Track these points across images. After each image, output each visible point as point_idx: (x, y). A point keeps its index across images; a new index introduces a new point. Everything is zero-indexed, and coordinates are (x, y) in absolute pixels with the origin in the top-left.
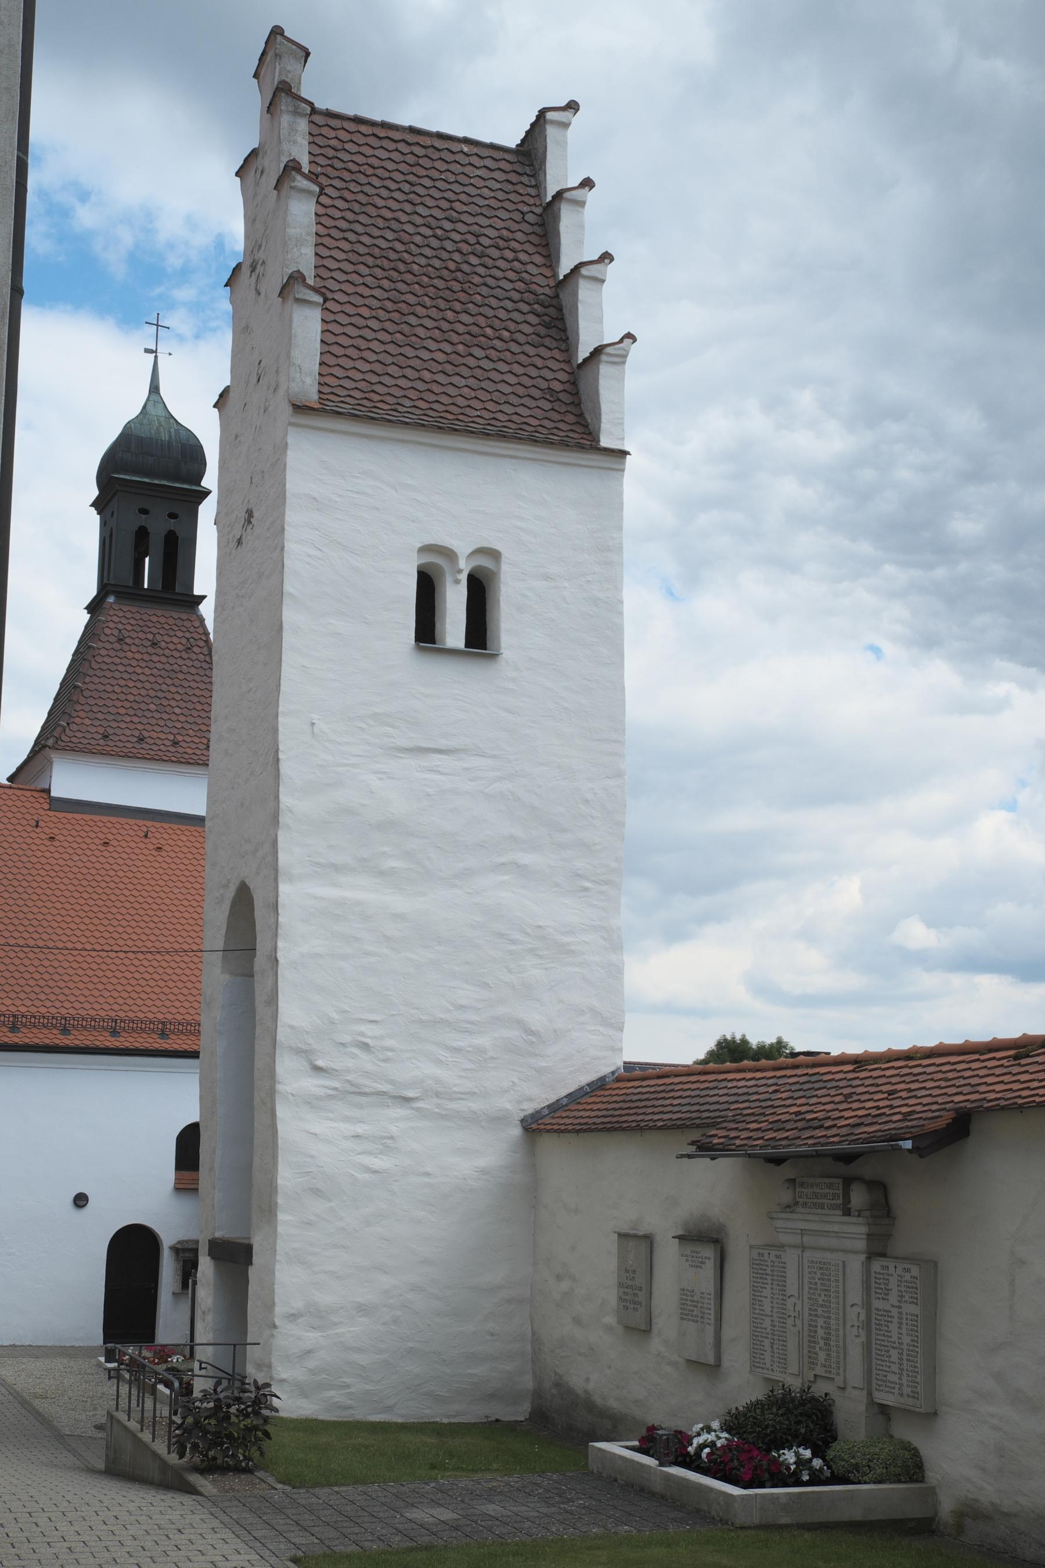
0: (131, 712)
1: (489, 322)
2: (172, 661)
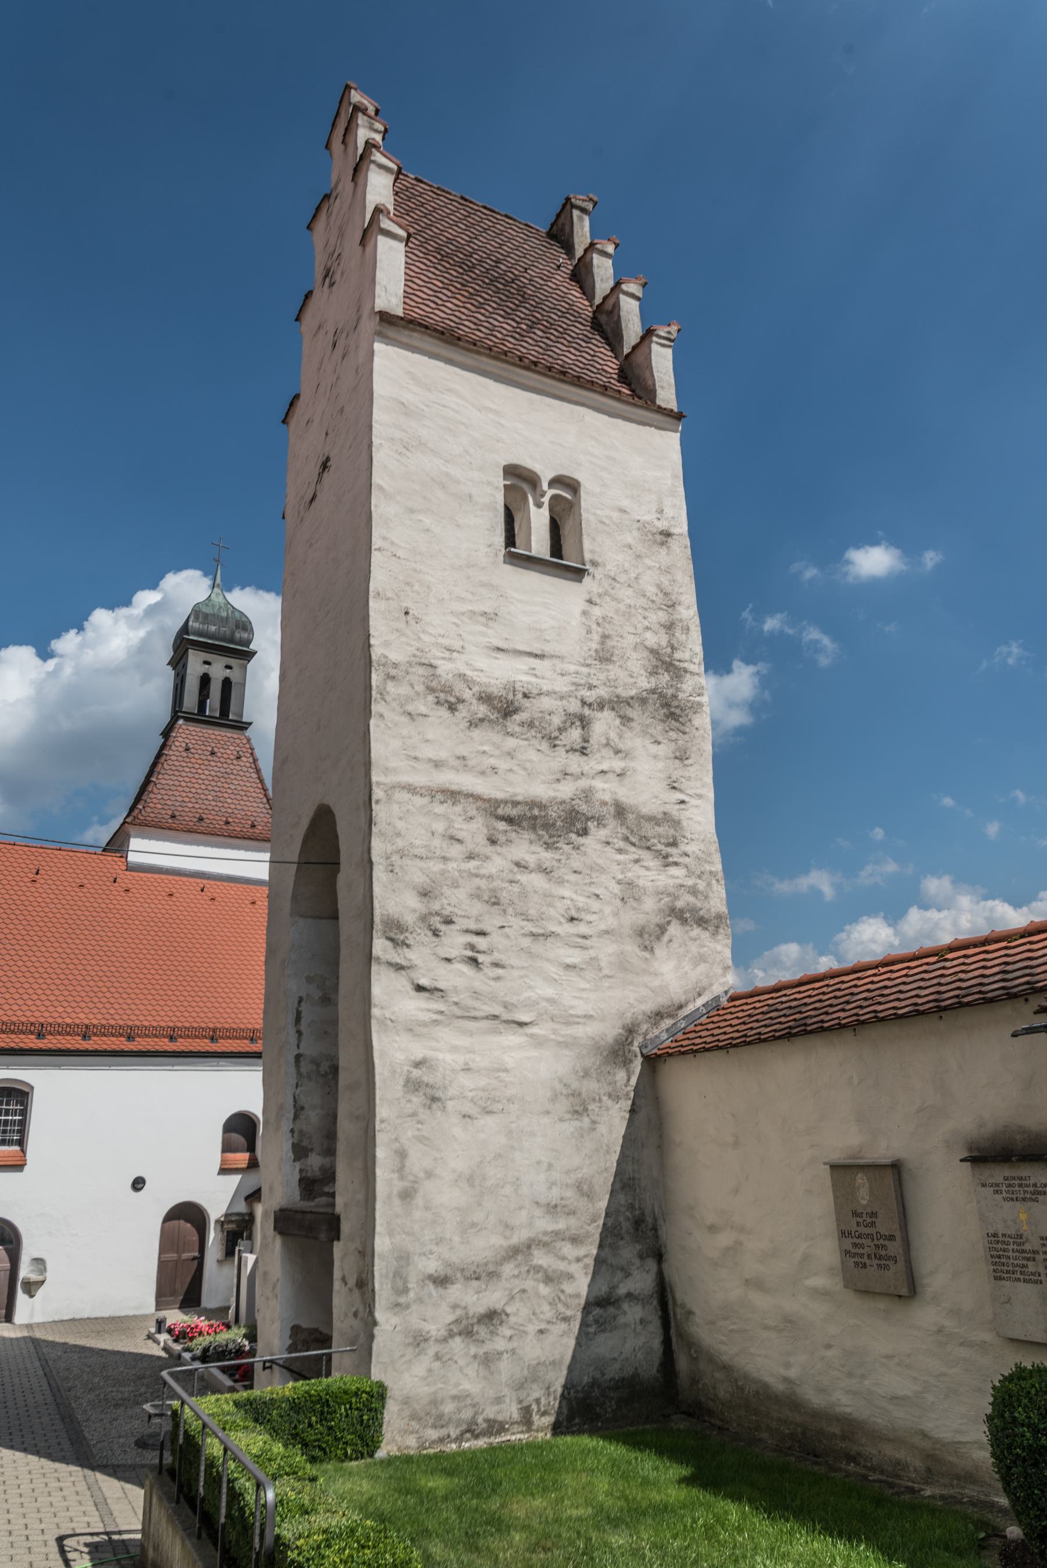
2: (225, 765)
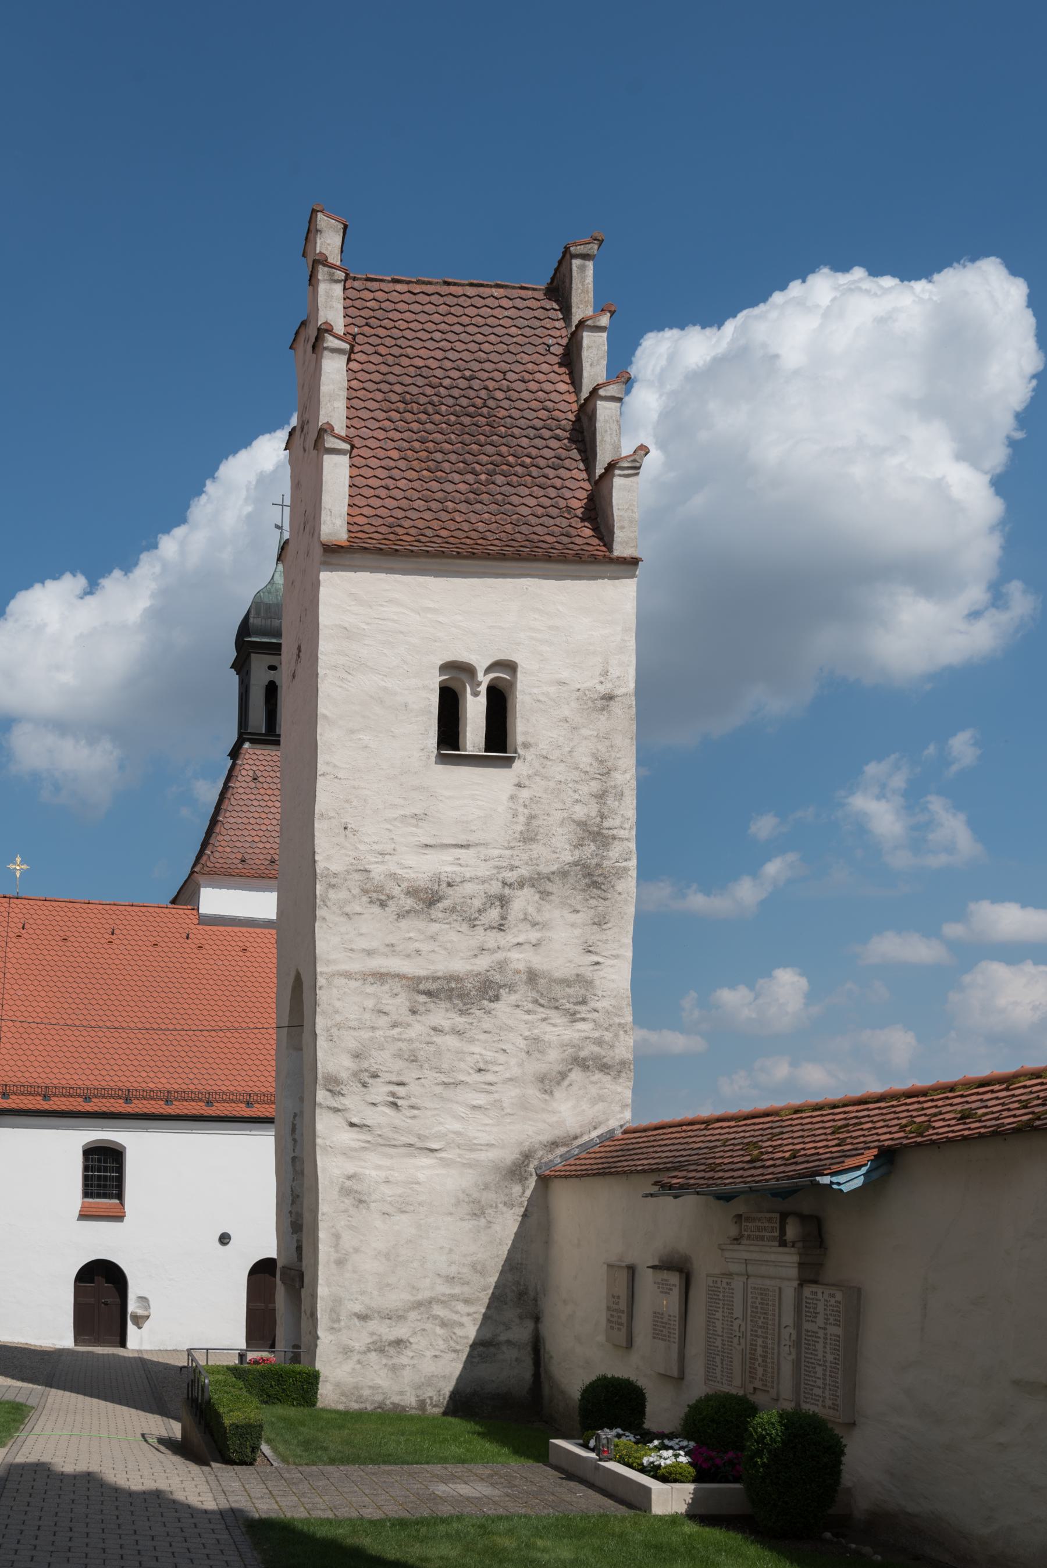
0: (264, 839)
1: (512, 451)
